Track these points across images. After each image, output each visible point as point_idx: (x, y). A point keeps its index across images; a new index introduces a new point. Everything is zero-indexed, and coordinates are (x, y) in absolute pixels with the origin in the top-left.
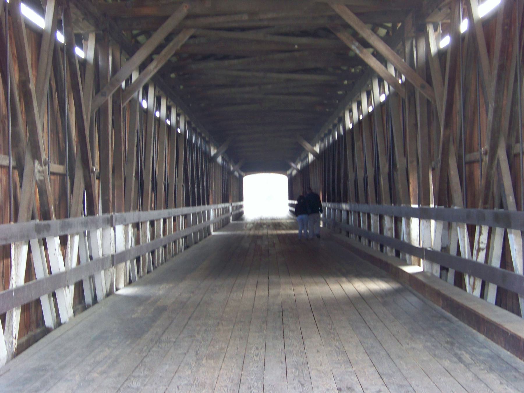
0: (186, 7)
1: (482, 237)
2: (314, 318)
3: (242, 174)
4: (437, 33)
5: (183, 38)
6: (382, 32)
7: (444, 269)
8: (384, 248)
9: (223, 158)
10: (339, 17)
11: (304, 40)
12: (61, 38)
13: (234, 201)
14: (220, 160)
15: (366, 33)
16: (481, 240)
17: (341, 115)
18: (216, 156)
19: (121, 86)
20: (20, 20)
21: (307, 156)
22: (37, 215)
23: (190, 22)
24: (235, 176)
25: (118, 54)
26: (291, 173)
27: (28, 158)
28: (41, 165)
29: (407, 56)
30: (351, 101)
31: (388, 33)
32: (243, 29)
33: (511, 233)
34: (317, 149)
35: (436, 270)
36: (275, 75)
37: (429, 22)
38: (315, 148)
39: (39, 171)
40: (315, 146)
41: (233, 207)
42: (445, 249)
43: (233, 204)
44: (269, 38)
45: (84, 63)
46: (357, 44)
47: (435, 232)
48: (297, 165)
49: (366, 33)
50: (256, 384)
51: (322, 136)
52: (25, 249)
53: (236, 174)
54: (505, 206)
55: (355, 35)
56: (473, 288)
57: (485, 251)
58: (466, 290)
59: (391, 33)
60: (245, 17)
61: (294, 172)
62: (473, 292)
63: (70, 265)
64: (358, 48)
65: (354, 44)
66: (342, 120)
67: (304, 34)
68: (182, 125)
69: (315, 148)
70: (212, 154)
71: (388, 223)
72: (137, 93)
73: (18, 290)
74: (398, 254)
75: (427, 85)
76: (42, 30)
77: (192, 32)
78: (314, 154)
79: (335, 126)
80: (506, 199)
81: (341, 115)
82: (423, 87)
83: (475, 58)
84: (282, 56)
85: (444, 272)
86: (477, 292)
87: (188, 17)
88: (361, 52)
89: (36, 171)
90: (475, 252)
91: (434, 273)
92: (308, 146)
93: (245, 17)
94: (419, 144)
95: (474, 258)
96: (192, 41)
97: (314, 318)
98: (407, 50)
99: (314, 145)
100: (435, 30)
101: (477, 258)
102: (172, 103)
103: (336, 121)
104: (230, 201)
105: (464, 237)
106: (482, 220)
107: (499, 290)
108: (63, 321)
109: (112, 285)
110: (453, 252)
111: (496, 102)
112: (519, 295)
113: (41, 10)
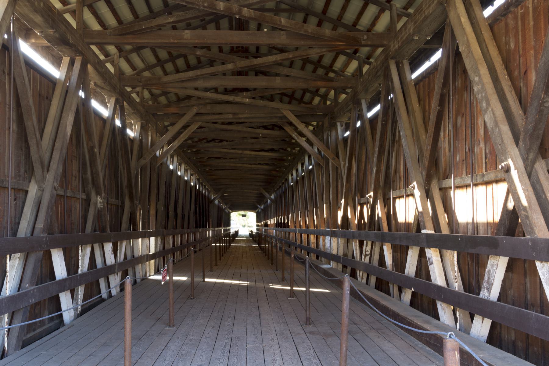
0: (195, 108)
1: (367, 248)
2: (58, 334)
3: (230, 211)
4: (342, 128)
5: (194, 127)
6: (311, 128)
7: (345, 267)
8: (310, 254)
9: (218, 201)
10: (285, 117)
11: (265, 131)
12: (118, 123)
13: (224, 227)
14: (216, 202)
15: (301, 127)
16: (367, 250)
17: (286, 177)
18: (214, 199)
19: (156, 154)
20: (127, 137)
21: (267, 201)
22: (97, 229)
23: (198, 118)
24: (225, 212)
25: (154, 135)
26: (258, 211)
27: (93, 194)
28: (102, 199)
29: (325, 142)
30: (292, 169)
31: (314, 129)
32: (230, 124)
33: (385, 245)
34: (272, 197)
35: (340, 266)
36: (249, 152)
37: (338, 121)
38: (271, 197)
39: (100, 203)
40: (272, 195)
41: (224, 230)
42: (345, 255)
43: (224, 228)
44: (245, 129)
45: (132, 140)
46: (296, 134)
47: (382, 159)
48: (261, 206)
49: (301, 127)
50: (227, 336)
51: (276, 189)
52: (88, 250)
53: (226, 211)
54: (381, 229)
55: (296, 129)
56: (362, 279)
57: (369, 256)
58: (357, 280)
59: (316, 129)
60: (231, 116)
61: (260, 210)
62: (362, 281)
63: (119, 260)
64: (296, 136)
65: (294, 134)
66: (287, 180)
67: (265, 128)
68: (194, 180)
69: (271, 197)
70: (212, 198)
71: (312, 238)
72: (166, 159)
73: (83, 275)
74: (317, 258)
75: (336, 159)
76: (56, 79)
77: (199, 124)
78: (271, 199)
79: (283, 183)
80: (382, 225)
81: (286, 177)
82: (333, 159)
83: (364, 141)
84: (253, 140)
85: (345, 269)
86: (364, 281)
87: (197, 114)
88: (298, 138)
89: (98, 202)
90: (363, 257)
91: (339, 268)
92: (267, 195)
93: (231, 116)
94: (331, 193)
95: (363, 260)
96: (199, 130)
97: (58, 334)
98: (325, 137)
99: (271, 195)
100: (342, 126)
101: (365, 260)
102: (188, 167)
103: (283, 181)
104: (223, 226)
105: (356, 246)
106: (368, 237)
107: (377, 279)
108: (113, 294)
109: (146, 273)
110: (350, 254)
111: (377, 167)
112: (389, 283)
113: (104, 103)
